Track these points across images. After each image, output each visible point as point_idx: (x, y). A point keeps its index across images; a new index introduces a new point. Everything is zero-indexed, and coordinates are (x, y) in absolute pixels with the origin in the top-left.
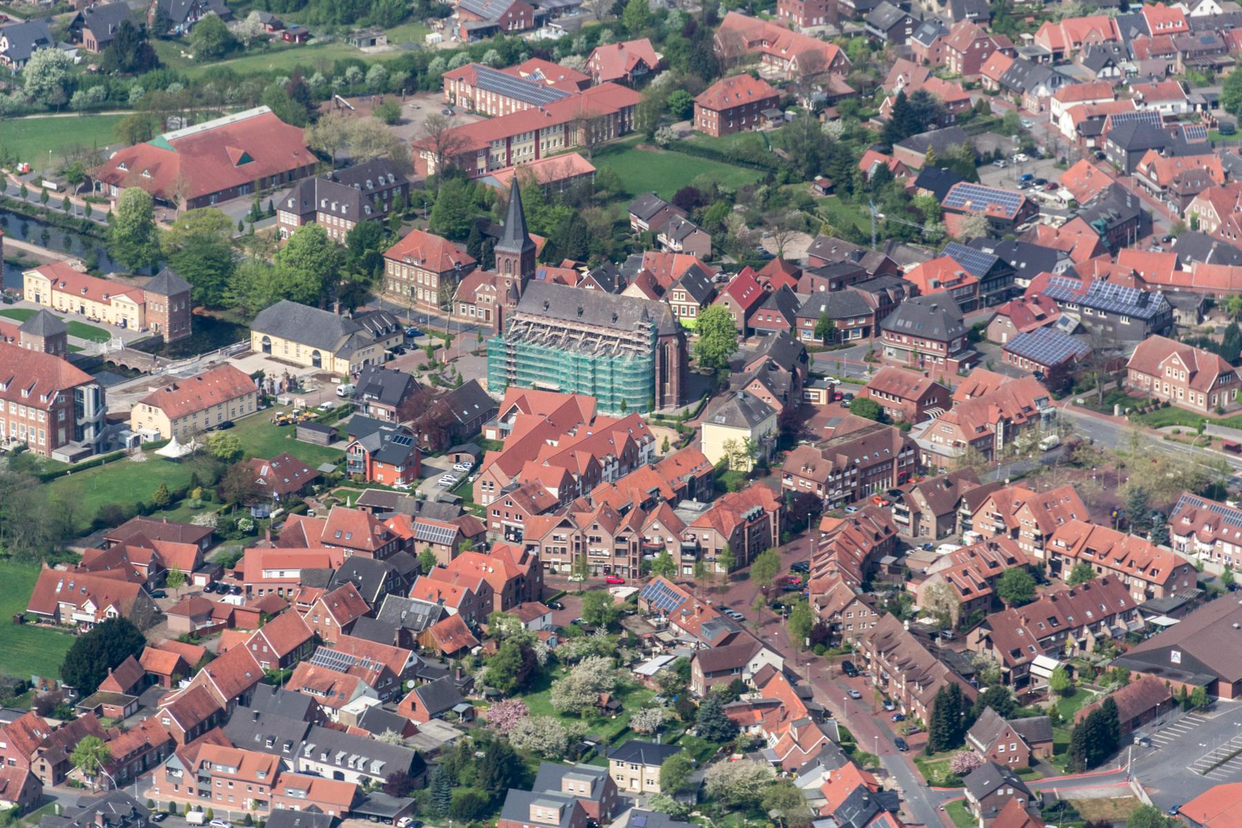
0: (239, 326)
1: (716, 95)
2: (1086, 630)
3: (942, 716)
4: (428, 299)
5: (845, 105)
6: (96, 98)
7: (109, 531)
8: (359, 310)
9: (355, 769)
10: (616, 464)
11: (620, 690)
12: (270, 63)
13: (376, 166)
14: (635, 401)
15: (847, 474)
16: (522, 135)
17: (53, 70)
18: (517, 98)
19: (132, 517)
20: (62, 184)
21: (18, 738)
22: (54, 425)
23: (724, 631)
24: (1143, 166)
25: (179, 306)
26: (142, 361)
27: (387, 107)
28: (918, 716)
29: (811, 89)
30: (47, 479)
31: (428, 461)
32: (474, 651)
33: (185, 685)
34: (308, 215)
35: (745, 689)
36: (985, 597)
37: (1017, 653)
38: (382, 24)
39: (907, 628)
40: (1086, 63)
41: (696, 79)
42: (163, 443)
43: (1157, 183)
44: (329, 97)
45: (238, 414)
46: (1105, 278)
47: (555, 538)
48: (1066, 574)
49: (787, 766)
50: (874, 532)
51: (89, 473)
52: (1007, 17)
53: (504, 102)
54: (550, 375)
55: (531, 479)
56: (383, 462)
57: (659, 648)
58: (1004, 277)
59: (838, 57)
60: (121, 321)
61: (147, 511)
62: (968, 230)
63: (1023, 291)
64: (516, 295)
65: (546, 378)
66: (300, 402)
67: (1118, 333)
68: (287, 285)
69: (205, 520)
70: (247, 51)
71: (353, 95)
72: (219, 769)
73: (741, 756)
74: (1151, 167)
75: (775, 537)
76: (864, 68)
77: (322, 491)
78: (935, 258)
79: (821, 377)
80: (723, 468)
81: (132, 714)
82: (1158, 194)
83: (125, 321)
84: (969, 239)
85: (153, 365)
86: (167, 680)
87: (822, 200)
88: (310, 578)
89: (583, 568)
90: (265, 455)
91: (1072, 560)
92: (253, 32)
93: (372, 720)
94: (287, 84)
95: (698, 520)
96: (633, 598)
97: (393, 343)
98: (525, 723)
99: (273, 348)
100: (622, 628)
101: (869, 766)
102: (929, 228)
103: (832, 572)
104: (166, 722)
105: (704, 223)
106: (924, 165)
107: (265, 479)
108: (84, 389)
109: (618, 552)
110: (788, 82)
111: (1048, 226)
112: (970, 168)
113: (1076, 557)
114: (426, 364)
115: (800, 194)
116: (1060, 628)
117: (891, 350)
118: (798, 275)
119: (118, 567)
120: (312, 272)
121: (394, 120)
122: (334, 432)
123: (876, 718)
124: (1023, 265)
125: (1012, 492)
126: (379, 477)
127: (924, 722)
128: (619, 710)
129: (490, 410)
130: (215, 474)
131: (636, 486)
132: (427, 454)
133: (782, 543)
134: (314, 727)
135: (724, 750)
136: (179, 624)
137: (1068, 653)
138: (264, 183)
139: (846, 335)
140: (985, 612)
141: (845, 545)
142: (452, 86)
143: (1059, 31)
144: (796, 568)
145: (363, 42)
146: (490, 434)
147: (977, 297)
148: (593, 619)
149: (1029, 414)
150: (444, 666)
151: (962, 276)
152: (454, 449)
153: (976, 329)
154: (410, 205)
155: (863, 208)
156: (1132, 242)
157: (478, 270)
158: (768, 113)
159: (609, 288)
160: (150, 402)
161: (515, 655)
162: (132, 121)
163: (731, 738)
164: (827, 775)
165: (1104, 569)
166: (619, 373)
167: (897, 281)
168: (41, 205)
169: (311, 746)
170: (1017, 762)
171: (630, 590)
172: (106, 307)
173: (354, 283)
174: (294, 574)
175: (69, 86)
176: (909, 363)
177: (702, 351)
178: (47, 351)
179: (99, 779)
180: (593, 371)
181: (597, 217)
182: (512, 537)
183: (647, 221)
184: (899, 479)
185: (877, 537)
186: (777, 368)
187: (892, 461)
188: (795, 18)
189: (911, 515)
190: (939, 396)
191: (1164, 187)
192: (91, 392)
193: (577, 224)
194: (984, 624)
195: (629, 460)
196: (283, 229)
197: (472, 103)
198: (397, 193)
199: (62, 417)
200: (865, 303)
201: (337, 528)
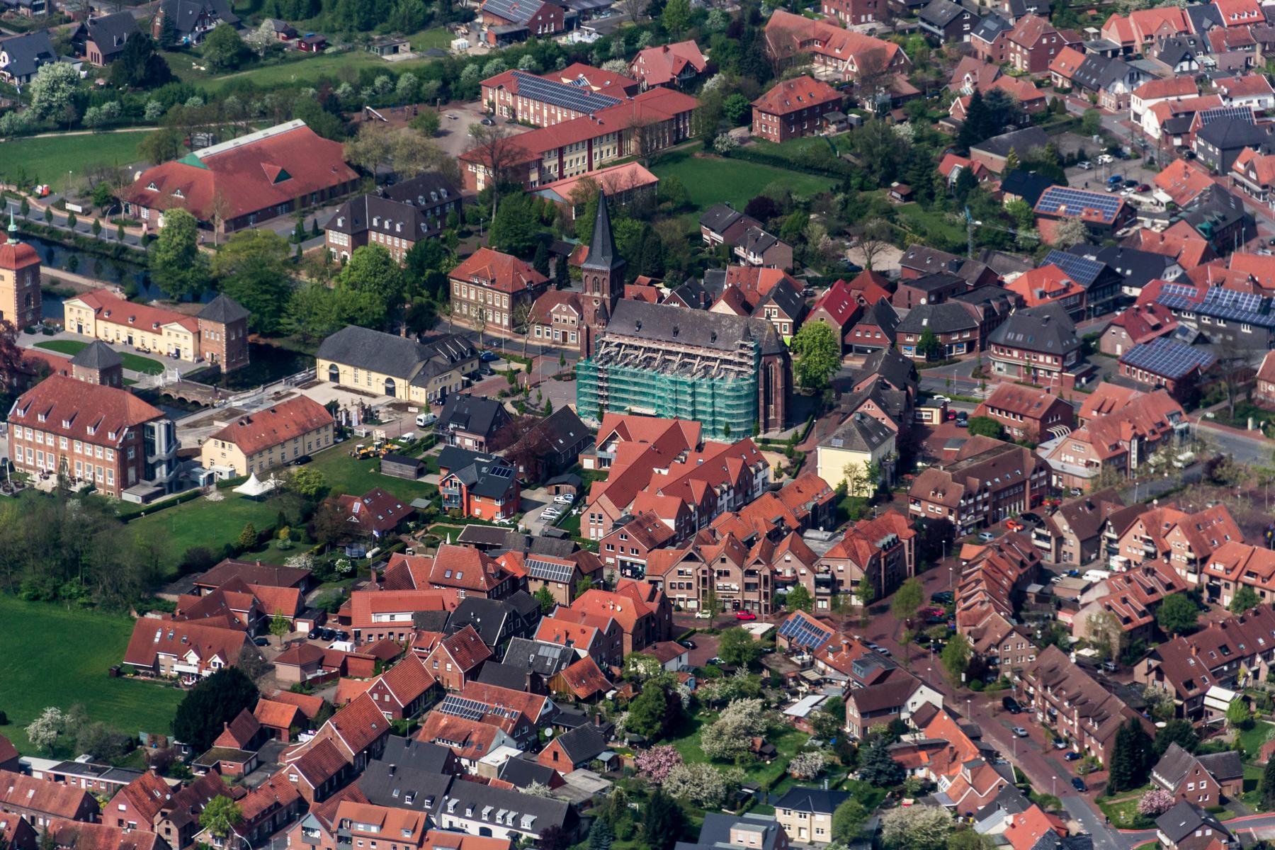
0: (299, 353)
1: (774, 95)
2: (1259, 659)
3: (1124, 753)
4: (499, 323)
5: (913, 107)
6: (110, 114)
7: (199, 576)
8: (428, 333)
9: (504, 825)
10: (732, 492)
11: (772, 734)
12: (291, 74)
13: (426, 182)
14: (739, 424)
15: (979, 498)
16: (574, 146)
17: (63, 85)
18: (563, 106)
19: (221, 560)
20: (87, 206)
21: (139, 799)
22: (123, 463)
23: (878, 668)
24: (1240, 165)
25: (237, 334)
26: (202, 394)
27: (423, 118)
28: (1093, 754)
29: (875, 91)
30: (125, 519)
31: (526, 494)
32: (609, 695)
33: (305, 738)
34: (359, 238)
35: (906, 730)
36: (1146, 626)
37: (1190, 685)
38: (402, 31)
39: (1073, 661)
40: (1161, 57)
41: (752, 82)
42: (242, 480)
43: (1257, 183)
44: (359, 108)
45: (314, 448)
46: (1220, 284)
47: (680, 573)
48: (1227, 599)
49: (962, 810)
50: (1019, 559)
51: (164, 513)
52: (1067, 10)
53: (549, 111)
54: (645, 399)
55: (646, 511)
56: (480, 496)
57: (805, 687)
58: (1112, 285)
59: (897, 55)
60: (173, 352)
61: (234, 552)
62: (1065, 236)
63: (1133, 300)
64: (605, 315)
65: (642, 403)
66: (379, 433)
67: (1239, 340)
68: (350, 311)
69: (300, 561)
70: (262, 61)
71: (383, 107)
72: (361, 828)
73: (911, 801)
74: (1250, 166)
75: (910, 566)
76: (924, 66)
77: (417, 528)
78: (1036, 267)
79: (931, 396)
80: (842, 493)
81: (251, 771)
82: (1258, 195)
83: (178, 351)
84: (1066, 246)
85: (215, 396)
86: (285, 735)
87: (900, 207)
88: (424, 621)
89: (711, 602)
90: (357, 492)
91: (1232, 585)
92: (268, 42)
93: (513, 771)
94: (314, 95)
95: (833, 551)
96: (769, 634)
97: (469, 369)
98: (679, 771)
99: (341, 377)
100: (762, 667)
101: (1051, 808)
102: (1022, 233)
103: (982, 603)
104: (294, 778)
105: (781, 234)
106: (1007, 169)
107: (358, 516)
108: (155, 425)
109: (748, 587)
110: (845, 83)
111: (1151, 228)
112: (1055, 171)
113: (1236, 582)
114: (507, 390)
115: (879, 201)
116: (1232, 657)
117: (1001, 366)
118: (892, 288)
119: (217, 615)
120: (377, 295)
121: (434, 131)
122: (422, 465)
123: (1048, 756)
124: (1129, 272)
125: (1161, 514)
126: (477, 512)
127: (1101, 760)
128: (773, 755)
129: (586, 439)
130: (301, 512)
131: (761, 515)
132: (526, 486)
133: (917, 572)
134: (457, 780)
135: (893, 795)
136: (289, 673)
137: (1242, 682)
138: (304, 201)
139: (950, 350)
140: (1147, 641)
141: (992, 574)
142: (490, 95)
143: (1129, 24)
144: (937, 599)
145: (386, 50)
146: (588, 464)
147: (1084, 307)
148: (732, 659)
149: (1163, 429)
150: (579, 712)
151: (1068, 284)
152: (552, 480)
153: (1087, 340)
154: (464, 221)
155: (948, 216)
156: (1240, 245)
157: (552, 289)
158: (831, 116)
159: (695, 305)
160: (223, 436)
161: (658, 699)
162: (157, 138)
163: (900, 782)
164: (1010, 819)
165: (1268, 594)
166: (720, 395)
167: (999, 291)
168: (67, 229)
169: (454, 801)
170: (1206, 800)
171: (765, 627)
172: (157, 336)
173: (421, 306)
174: (405, 618)
175: (81, 103)
176: (1022, 379)
177: (804, 371)
178: (102, 382)
179: (229, 841)
180: (693, 395)
181: (670, 229)
182: (628, 572)
183: (721, 234)
184: (1031, 502)
185: (1022, 564)
186: (889, 387)
187: (1024, 483)
188: (841, 15)
189: (1053, 540)
190: (1064, 414)
191: (1264, 187)
192: (163, 428)
193: (651, 238)
194: (1154, 655)
195: (745, 490)
196: (332, 250)
197: (513, 112)
198: (450, 209)
199: (131, 455)
200: (970, 316)
201: (444, 567)
